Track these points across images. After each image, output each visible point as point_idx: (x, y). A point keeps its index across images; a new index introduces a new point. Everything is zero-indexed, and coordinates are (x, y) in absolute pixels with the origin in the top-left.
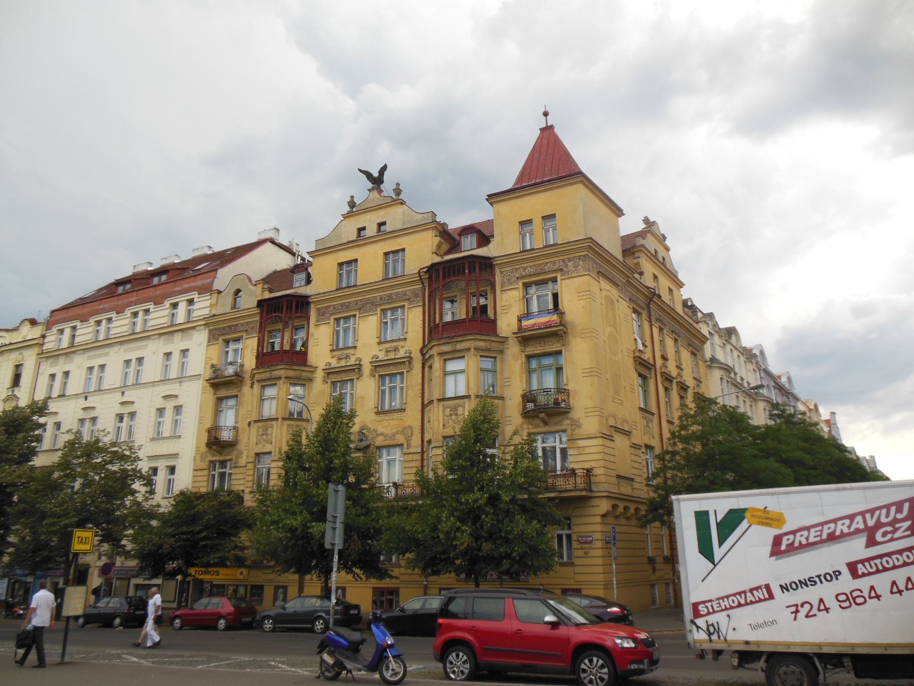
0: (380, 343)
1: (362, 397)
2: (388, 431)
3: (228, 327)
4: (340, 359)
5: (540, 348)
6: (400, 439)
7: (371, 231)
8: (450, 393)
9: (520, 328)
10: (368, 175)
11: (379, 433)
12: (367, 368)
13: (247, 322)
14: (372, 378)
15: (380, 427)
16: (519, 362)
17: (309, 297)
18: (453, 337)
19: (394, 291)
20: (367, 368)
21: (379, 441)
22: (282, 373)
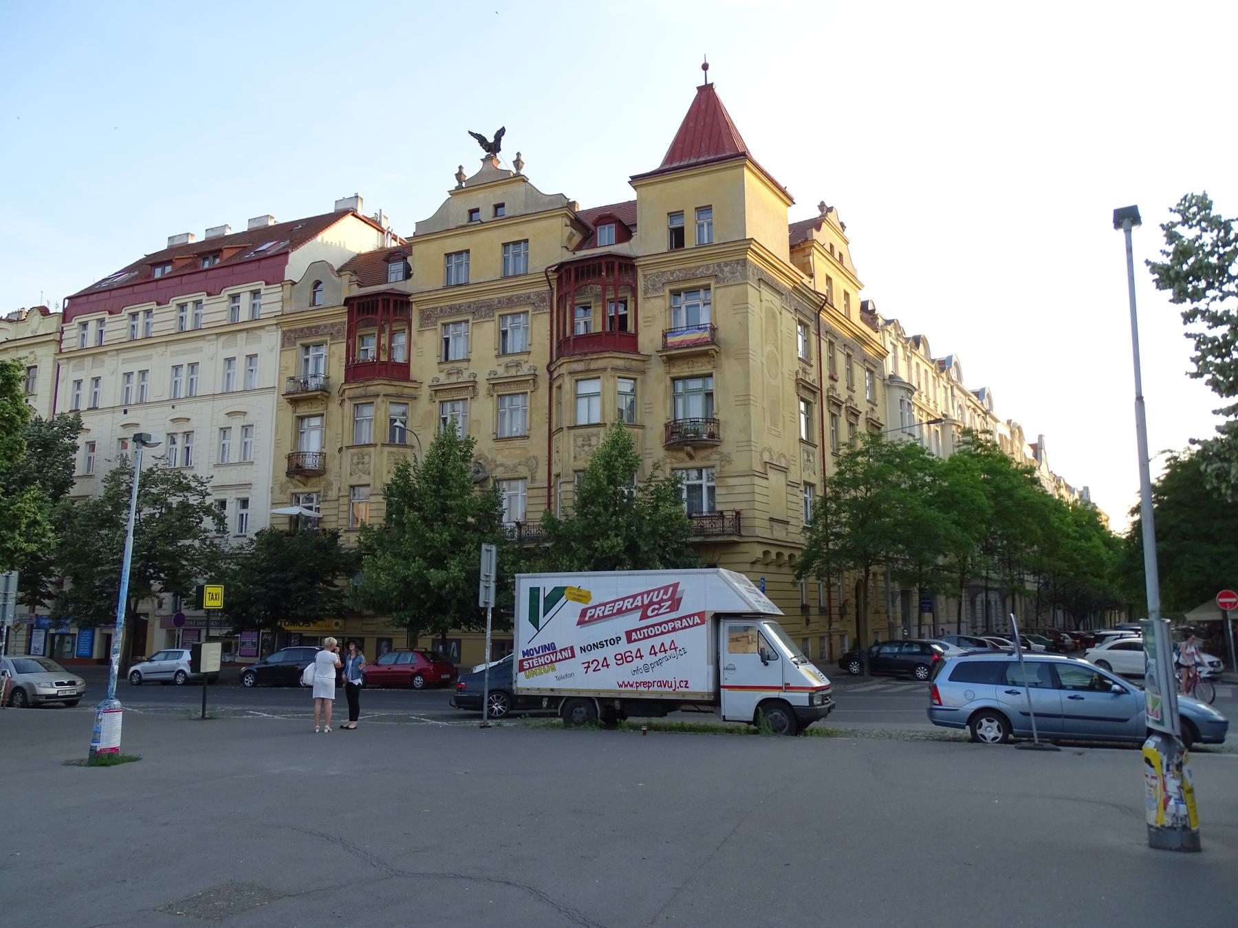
0: (498, 356)
2: (510, 462)
4: (449, 374)
5: (688, 370)
7: (486, 214)
8: (582, 421)
9: (665, 346)
10: (482, 140)
12: (483, 388)
15: (500, 456)
16: (663, 385)
17: (410, 295)
18: (586, 354)
19: (515, 293)
20: (483, 388)
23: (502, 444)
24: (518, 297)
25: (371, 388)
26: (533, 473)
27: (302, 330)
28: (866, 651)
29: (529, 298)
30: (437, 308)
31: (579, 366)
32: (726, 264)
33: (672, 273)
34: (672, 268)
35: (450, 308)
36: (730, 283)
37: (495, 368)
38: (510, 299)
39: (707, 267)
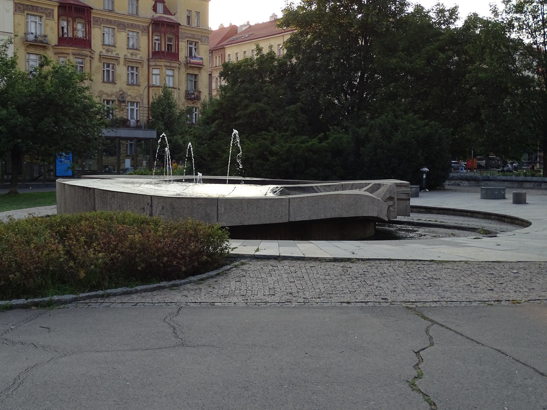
1: (120, 75)
2: (133, 95)
3: (31, 5)
4: (132, 54)
6: (138, 99)
11: (128, 94)
12: (122, 61)
13: (46, 8)
14: (125, 66)
15: (129, 92)
16: (185, 75)
17: (92, 9)
18: (171, 60)
19: (135, 23)
20: (122, 61)
21: (128, 99)
22: (162, 64)
23: (130, 87)
24: (135, 25)
25: (84, 52)
26: (142, 100)
27: (27, 5)
28: (530, 72)
29: (139, 27)
30: (100, 18)
31: (168, 64)
32: (204, 36)
33: (188, 34)
34: (188, 32)
35: (107, 20)
36: (204, 43)
37: (126, 53)
38: (132, 24)
39: (198, 35)
